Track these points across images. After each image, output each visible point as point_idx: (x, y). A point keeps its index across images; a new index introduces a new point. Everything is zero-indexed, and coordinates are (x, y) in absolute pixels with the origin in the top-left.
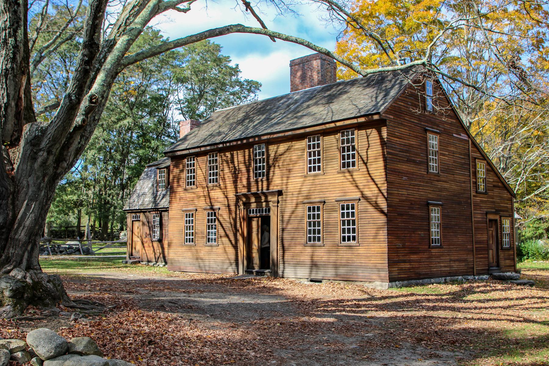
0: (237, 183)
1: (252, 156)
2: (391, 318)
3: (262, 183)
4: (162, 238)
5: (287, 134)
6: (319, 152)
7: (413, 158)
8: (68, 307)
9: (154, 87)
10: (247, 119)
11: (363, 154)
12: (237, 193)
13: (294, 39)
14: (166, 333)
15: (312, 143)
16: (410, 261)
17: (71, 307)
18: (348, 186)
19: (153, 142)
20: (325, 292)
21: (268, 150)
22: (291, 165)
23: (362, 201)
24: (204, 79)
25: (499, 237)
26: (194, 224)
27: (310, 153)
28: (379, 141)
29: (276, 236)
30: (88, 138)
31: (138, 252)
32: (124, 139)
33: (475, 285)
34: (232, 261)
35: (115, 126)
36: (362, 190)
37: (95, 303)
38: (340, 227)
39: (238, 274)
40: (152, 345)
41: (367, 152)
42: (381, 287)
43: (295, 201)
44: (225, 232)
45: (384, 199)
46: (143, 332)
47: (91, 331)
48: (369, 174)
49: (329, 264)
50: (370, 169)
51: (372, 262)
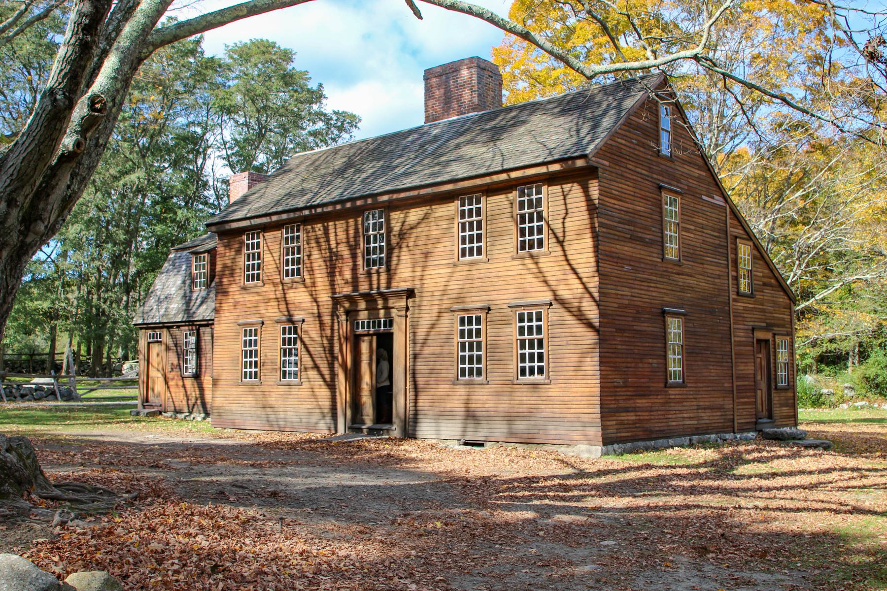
0: (335, 276)
1: (361, 230)
2: (630, 509)
3: (379, 276)
4: (200, 371)
5: (423, 192)
6: (479, 223)
7: (640, 235)
8: (46, 498)
9: (181, 120)
10: (351, 167)
11: (557, 226)
12: (334, 293)
13: (466, 7)
14: (241, 547)
15: (467, 208)
16: (635, 410)
17: (53, 499)
18: (530, 280)
19: (179, 212)
20: (495, 462)
21: (388, 221)
22: (430, 246)
23: (554, 306)
24: (265, 108)
25: (772, 369)
26: (258, 348)
27: (463, 225)
28: (584, 204)
29: (403, 367)
30: (84, 178)
31: (159, 395)
32: (130, 206)
33: (741, 448)
34: (326, 411)
35: (115, 184)
36: (554, 288)
37: (96, 490)
38: (517, 351)
39: (336, 432)
40: (218, 573)
41: (563, 223)
42: (590, 453)
43: (436, 307)
44: (314, 361)
45: (593, 303)
46: (195, 547)
47: (95, 546)
48: (567, 260)
49: (496, 414)
50: (568, 253)
51: (572, 411)
